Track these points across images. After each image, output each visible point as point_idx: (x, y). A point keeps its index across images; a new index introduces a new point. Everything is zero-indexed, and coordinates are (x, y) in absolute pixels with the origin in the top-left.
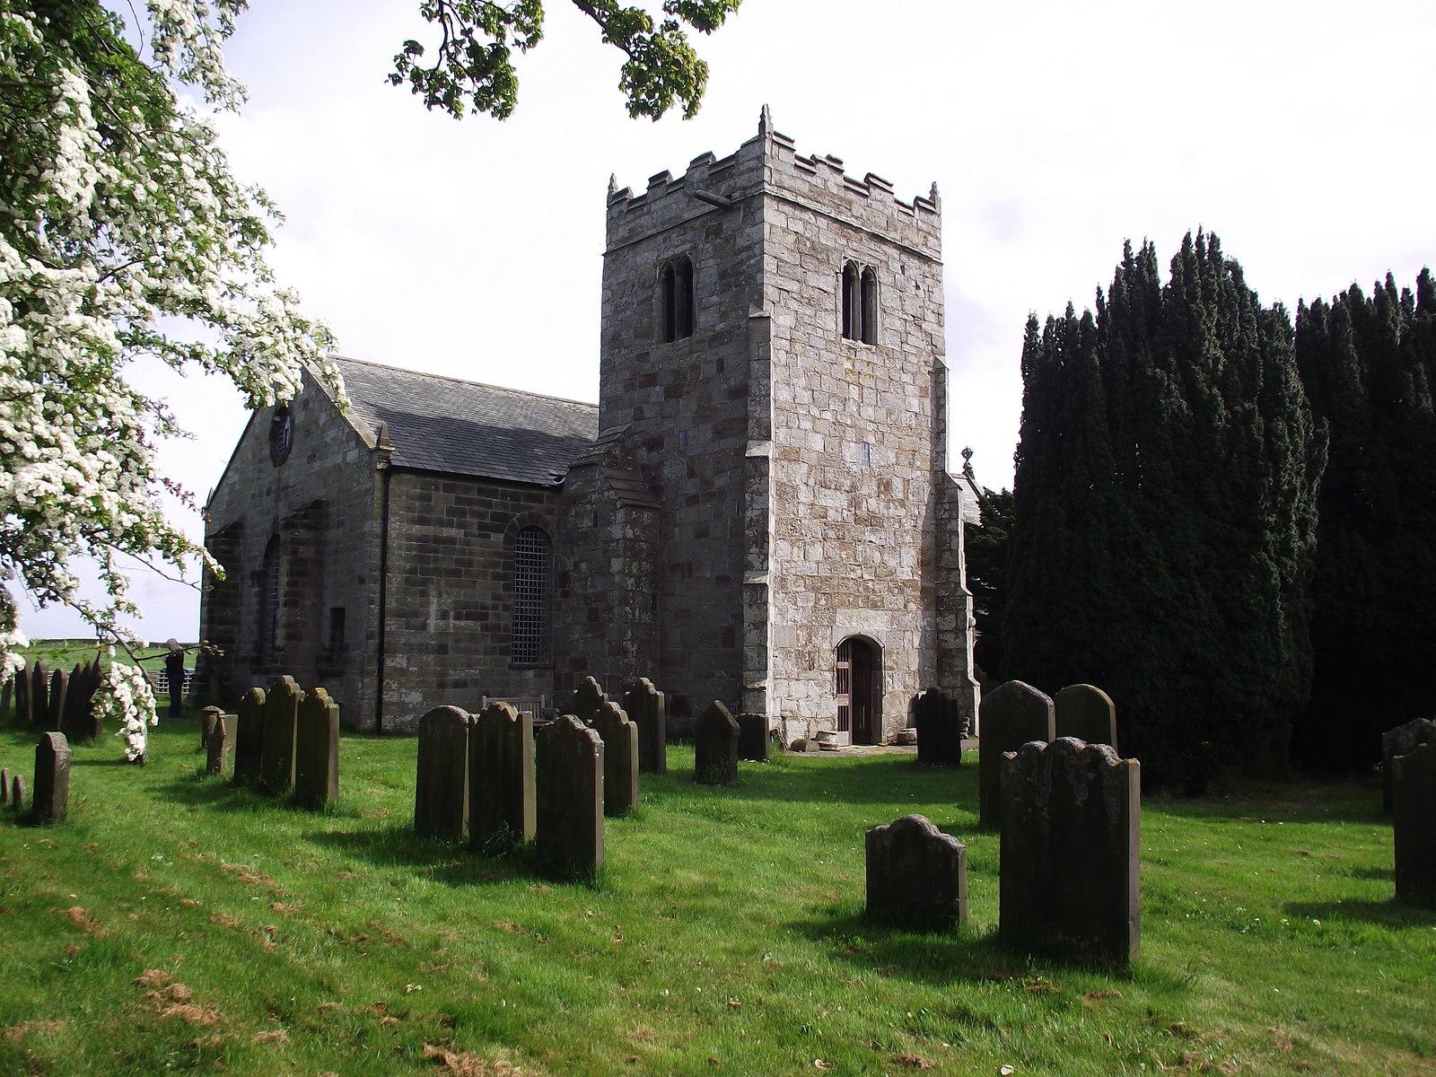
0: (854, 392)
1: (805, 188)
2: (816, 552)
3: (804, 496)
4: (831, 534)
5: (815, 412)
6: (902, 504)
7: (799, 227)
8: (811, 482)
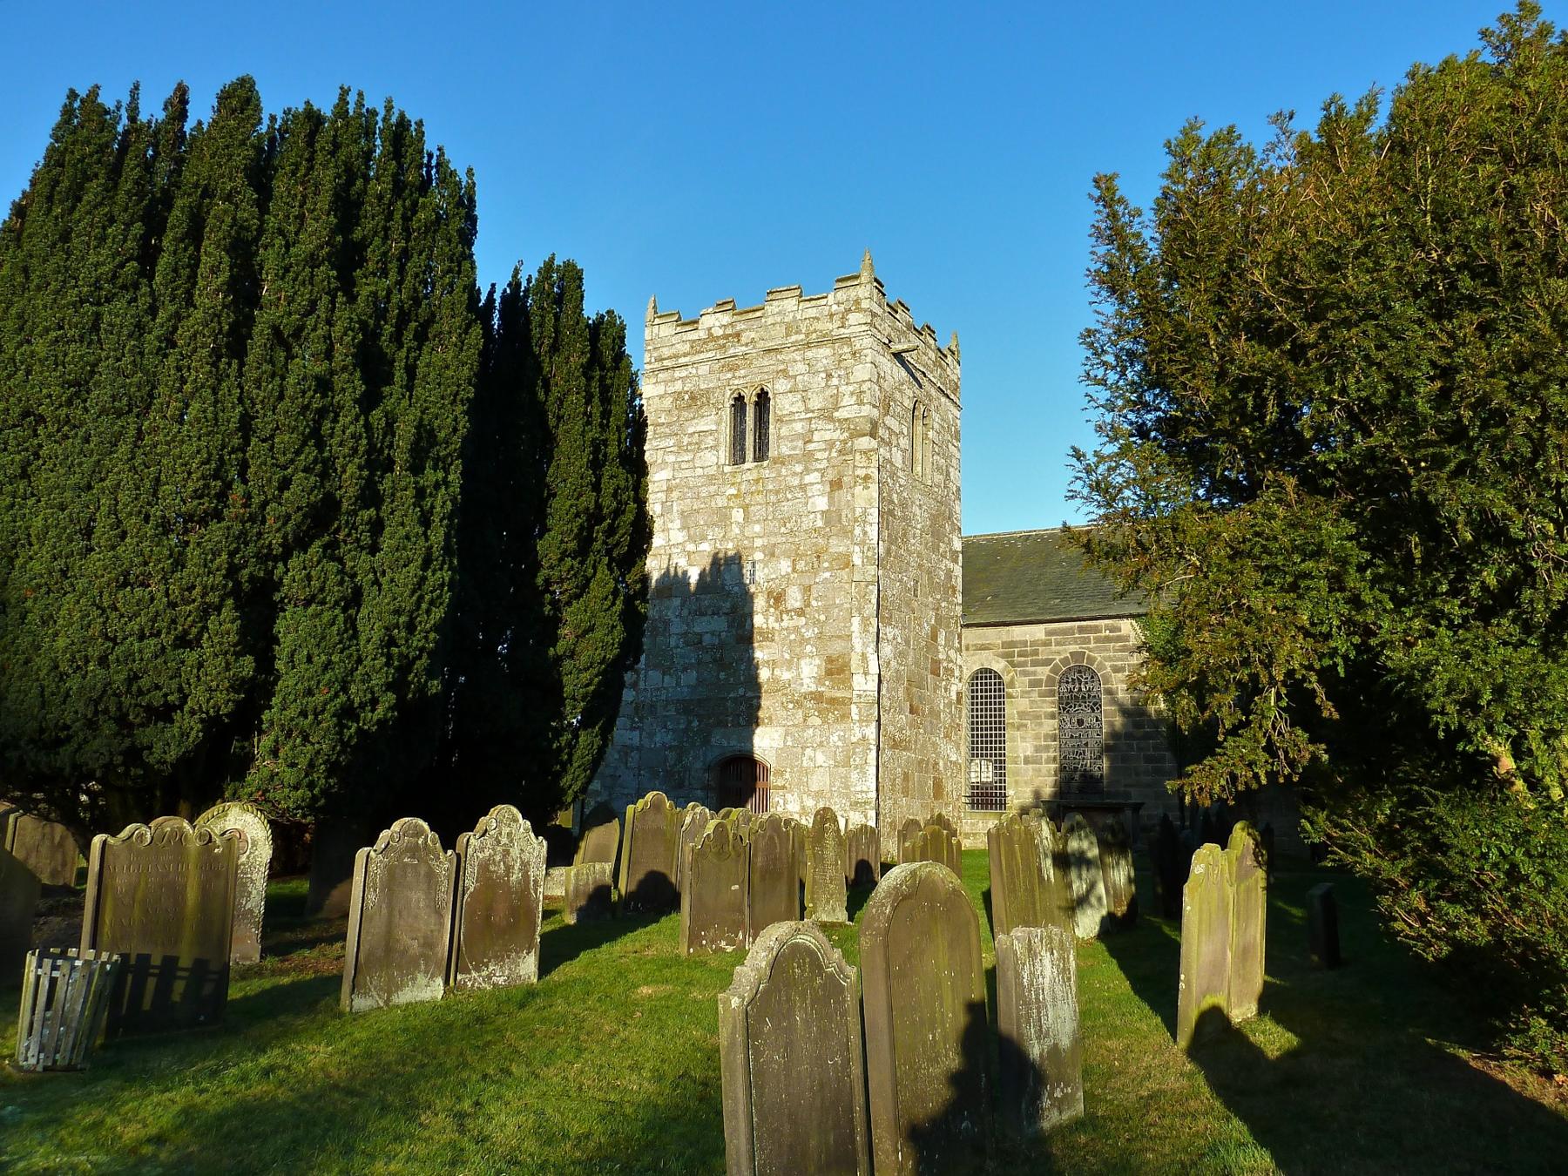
0: (738, 515)
1: (687, 348)
2: (691, 677)
3: (677, 628)
4: (707, 658)
5: (690, 547)
6: (801, 612)
7: (678, 386)
8: (685, 613)
